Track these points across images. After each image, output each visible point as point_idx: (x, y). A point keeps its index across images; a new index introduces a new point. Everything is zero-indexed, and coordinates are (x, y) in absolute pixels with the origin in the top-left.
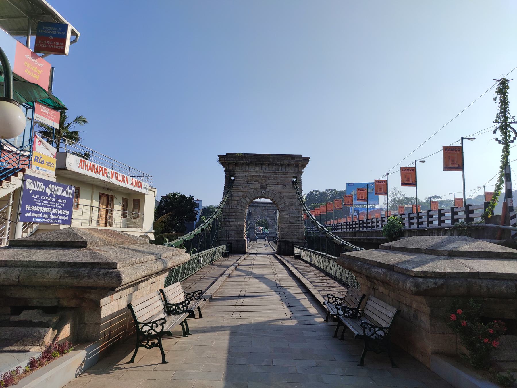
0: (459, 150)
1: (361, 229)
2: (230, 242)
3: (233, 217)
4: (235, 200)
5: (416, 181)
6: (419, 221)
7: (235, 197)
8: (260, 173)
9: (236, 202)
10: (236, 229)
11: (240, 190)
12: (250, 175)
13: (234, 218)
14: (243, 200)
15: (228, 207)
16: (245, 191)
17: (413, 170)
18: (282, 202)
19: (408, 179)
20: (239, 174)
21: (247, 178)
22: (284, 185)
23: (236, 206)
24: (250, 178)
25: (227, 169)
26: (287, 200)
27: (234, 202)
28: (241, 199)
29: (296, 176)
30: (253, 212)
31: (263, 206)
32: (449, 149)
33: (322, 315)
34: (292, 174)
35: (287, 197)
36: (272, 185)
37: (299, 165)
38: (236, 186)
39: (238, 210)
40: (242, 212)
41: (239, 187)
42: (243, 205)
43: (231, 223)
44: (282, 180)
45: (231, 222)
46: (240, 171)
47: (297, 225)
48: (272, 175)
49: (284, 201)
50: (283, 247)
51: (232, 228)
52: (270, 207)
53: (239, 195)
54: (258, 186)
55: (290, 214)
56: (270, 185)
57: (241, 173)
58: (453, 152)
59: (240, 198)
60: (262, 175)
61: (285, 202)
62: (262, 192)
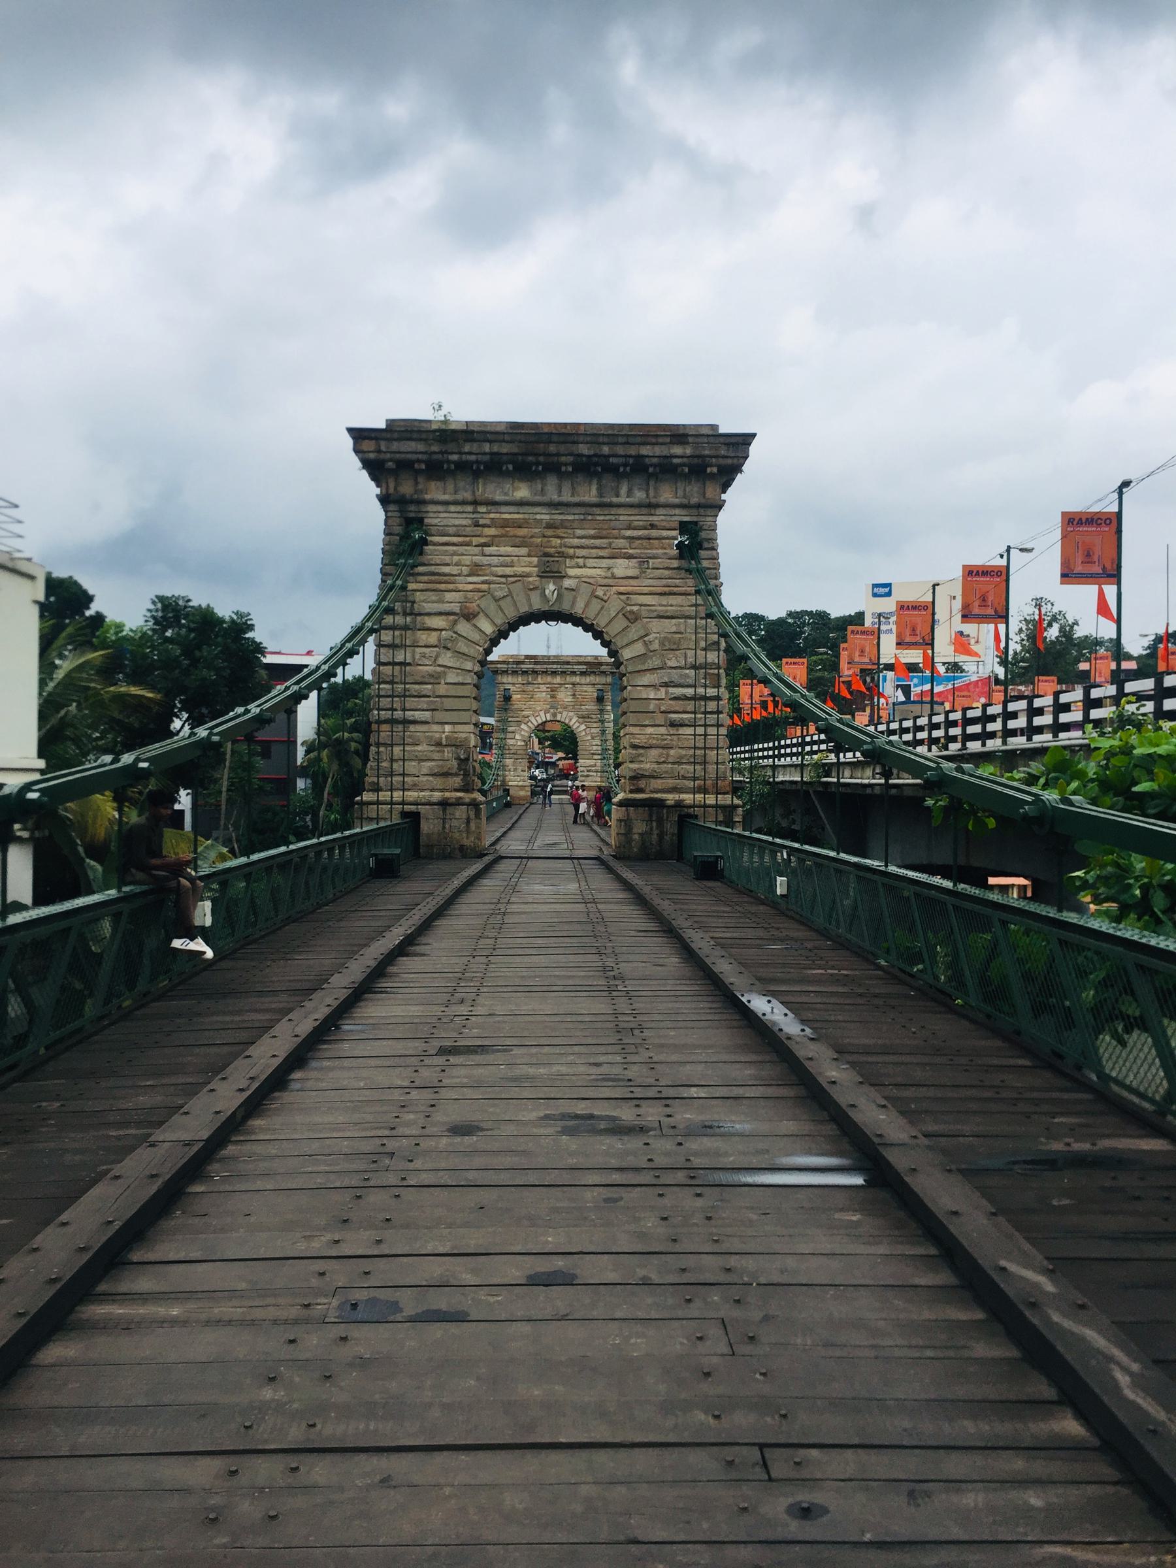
0: (1108, 522)
1: (954, 747)
2: (413, 808)
3: (423, 703)
4: (429, 629)
5: (1119, 567)
6: (1035, 724)
7: (429, 614)
8: (537, 509)
9: (433, 638)
10: (436, 756)
11: (451, 586)
12: (492, 516)
13: (425, 706)
14: (463, 627)
15: (400, 658)
16: (471, 587)
17: (1113, 523)
18: (633, 633)
19: (1088, 557)
20: (442, 515)
21: (479, 533)
22: (643, 561)
23: (434, 655)
24: (492, 531)
25: (391, 491)
26: (656, 625)
27: (423, 637)
28: (455, 622)
29: (694, 519)
30: (519, 696)
31: (554, 673)
32: (1081, 519)
33: (807, 1127)
34: (677, 511)
35: (655, 614)
36: (590, 562)
37: (709, 470)
38: (433, 568)
39: (445, 673)
40: (460, 679)
41: (446, 570)
42: (464, 649)
43: (412, 728)
44: (631, 539)
45: (415, 722)
46: (446, 497)
47: (700, 730)
48: (590, 517)
49: (642, 633)
50: (639, 827)
51: (419, 748)
52: (583, 673)
53: (446, 607)
54: (527, 565)
55: (666, 685)
56: (581, 561)
57: (452, 508)
58: (1090, 529)
59: (451, 618)
60: (543, 517)
61: (646, 635)
62: (547, 592)
